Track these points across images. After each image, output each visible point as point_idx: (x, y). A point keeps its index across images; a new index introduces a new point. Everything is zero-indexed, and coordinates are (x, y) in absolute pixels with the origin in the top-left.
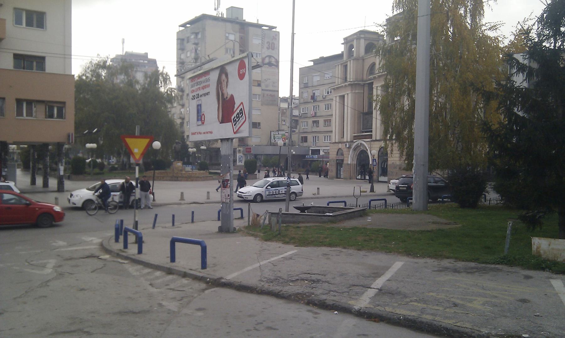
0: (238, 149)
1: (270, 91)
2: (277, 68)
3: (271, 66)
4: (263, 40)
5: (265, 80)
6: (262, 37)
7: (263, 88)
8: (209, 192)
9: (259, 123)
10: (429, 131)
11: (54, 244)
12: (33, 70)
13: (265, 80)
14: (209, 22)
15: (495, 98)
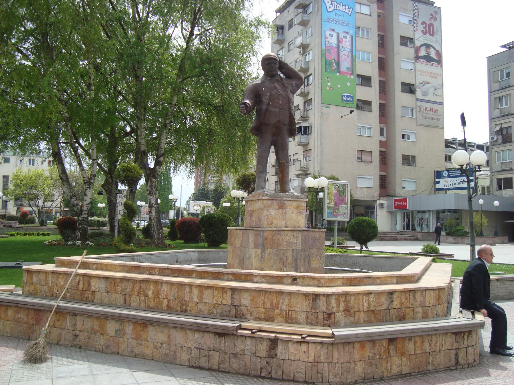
0: (378, 201)
1: (430, 102)
2: (439, 66)
3: (430, 62)
4: (415, 18)
5: (422, 83)
7: (418, 98)
8: (305, 133)
9: (414, 157)
10: (277, 291)
12: (33, 223)
13: (422, 83)
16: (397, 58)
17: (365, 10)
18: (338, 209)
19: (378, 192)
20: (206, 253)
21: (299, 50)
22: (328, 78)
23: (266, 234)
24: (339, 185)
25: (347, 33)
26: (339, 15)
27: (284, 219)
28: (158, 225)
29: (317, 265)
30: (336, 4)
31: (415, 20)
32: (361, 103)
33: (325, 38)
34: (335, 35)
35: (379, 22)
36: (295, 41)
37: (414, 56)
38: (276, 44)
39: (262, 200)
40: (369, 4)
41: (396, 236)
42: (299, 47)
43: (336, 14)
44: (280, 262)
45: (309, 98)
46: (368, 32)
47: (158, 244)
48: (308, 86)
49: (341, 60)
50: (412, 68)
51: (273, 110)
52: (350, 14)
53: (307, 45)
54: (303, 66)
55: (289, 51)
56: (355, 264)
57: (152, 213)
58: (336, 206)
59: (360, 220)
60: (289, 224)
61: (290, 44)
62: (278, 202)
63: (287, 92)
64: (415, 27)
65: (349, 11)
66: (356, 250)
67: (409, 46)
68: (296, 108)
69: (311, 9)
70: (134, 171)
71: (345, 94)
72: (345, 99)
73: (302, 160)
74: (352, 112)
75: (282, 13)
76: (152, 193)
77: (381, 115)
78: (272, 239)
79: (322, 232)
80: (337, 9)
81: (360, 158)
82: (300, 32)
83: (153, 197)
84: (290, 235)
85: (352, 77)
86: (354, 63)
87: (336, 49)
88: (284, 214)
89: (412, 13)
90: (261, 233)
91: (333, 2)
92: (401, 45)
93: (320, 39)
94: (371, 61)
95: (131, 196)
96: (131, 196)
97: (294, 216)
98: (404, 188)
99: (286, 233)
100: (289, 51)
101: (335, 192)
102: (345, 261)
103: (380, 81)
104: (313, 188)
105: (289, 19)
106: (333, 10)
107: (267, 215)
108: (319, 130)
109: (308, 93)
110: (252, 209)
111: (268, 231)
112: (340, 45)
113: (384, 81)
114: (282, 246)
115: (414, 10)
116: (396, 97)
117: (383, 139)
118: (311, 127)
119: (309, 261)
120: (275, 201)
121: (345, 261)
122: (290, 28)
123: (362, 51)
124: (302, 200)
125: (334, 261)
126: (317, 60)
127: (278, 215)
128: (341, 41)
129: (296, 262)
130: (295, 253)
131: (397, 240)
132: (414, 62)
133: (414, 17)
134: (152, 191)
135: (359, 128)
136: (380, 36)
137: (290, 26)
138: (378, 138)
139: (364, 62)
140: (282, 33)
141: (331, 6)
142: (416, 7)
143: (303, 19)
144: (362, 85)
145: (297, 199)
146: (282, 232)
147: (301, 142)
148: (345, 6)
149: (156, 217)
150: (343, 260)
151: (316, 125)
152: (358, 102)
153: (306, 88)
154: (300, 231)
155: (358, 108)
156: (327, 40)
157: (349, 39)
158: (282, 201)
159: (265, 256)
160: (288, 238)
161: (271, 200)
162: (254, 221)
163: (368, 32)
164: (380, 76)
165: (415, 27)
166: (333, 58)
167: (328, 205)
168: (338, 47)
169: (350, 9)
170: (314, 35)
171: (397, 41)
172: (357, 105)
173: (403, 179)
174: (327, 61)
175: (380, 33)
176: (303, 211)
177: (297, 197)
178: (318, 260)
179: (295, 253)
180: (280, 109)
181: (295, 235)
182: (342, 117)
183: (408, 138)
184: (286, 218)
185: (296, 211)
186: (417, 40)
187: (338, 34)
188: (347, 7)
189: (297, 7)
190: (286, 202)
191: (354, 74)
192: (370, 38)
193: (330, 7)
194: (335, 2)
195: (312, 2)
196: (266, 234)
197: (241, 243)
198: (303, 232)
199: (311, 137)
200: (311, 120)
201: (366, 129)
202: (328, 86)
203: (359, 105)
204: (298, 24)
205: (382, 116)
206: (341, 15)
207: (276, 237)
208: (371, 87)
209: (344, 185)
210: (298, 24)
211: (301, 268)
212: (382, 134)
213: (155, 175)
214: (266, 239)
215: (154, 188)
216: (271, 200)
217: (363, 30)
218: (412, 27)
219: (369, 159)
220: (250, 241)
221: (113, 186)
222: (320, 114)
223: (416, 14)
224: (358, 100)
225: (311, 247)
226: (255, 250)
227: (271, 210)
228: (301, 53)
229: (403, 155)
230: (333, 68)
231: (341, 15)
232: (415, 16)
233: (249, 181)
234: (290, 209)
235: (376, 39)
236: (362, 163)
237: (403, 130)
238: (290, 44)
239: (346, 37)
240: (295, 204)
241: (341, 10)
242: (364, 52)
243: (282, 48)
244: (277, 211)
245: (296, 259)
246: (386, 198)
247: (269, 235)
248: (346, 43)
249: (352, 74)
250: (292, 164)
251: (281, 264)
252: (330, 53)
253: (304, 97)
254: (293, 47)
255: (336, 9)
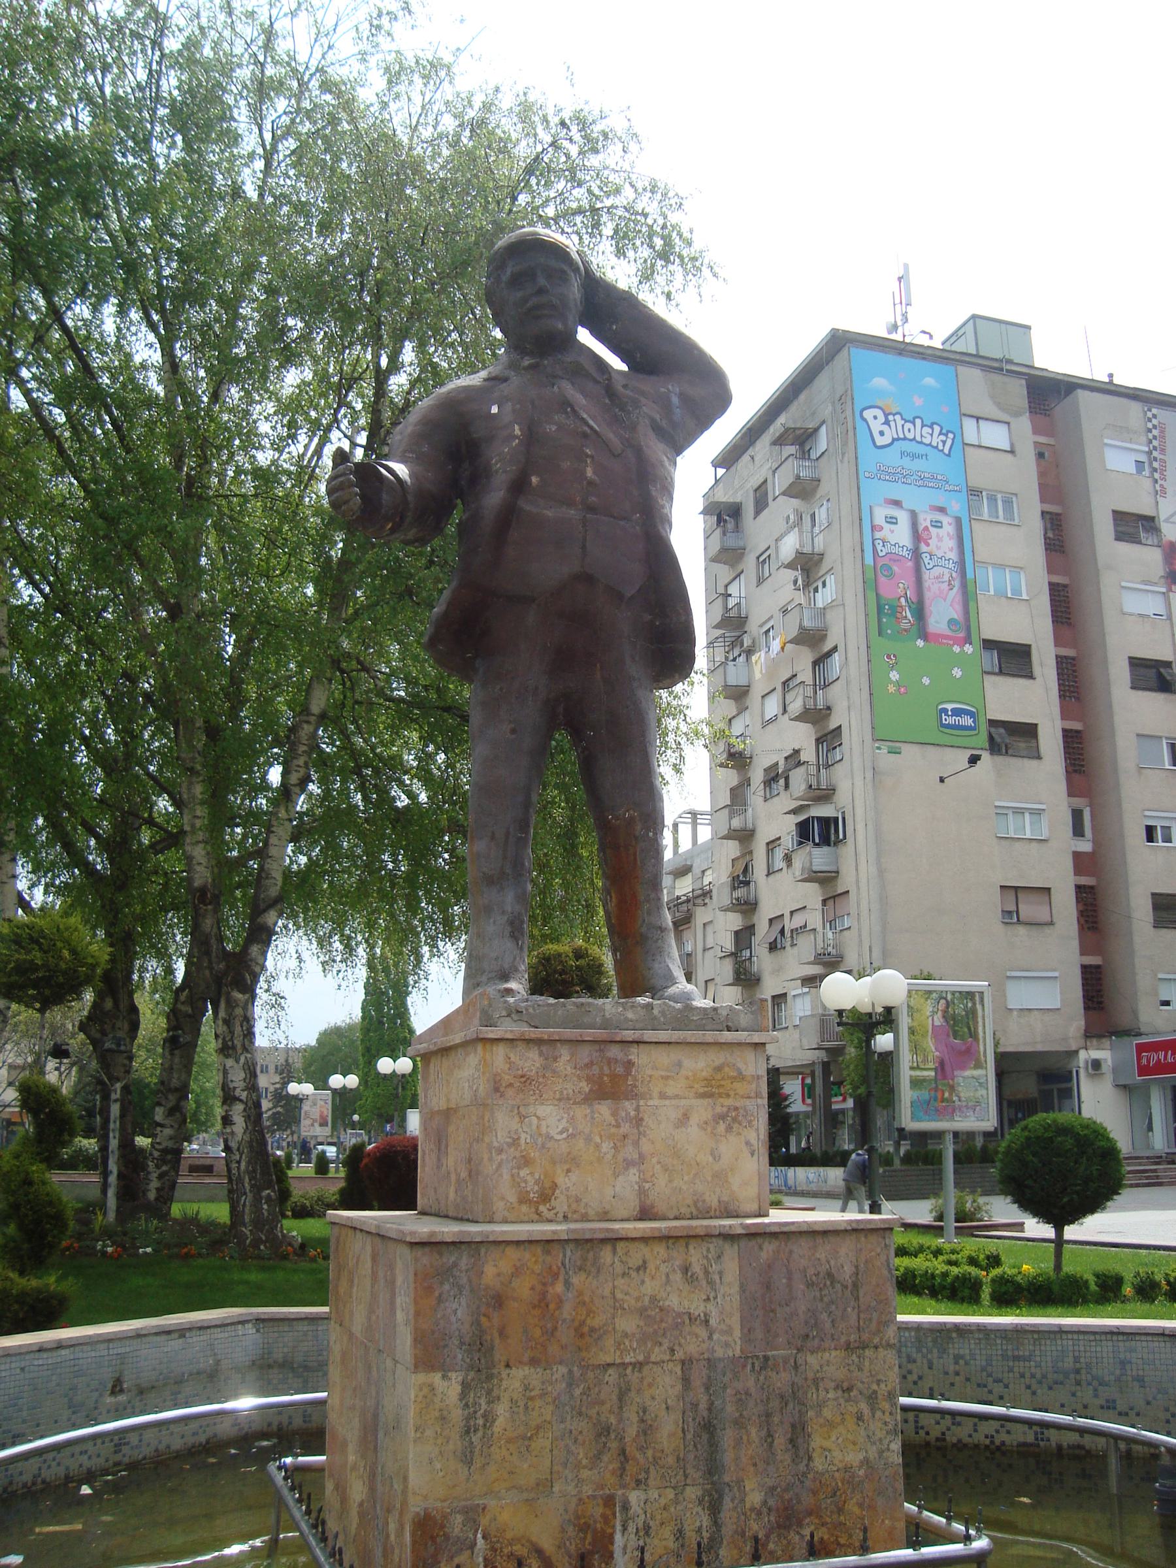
0: (1083, 1055)
4: (1155, 454)
6: (1150, 442)
8: (825, 841)
11: (266, 1538)
14: (859, 356)
15: (320, 1276)
16: (1108, 583)
17: (995, 435)
18: (952, 1088)
19: (1077, 1024)
20: (303, 1327)
21: (790, 575)
22: (889, 657)
23: (493, 1270)
24: (949, 997)
25: (942, 510)
26: (914, 456)
27: (629, 1164)
28: (254, 1171)
29: (853, 1458)
30: (900, 422)
31: (1155, 459)
32: (1002, 730)
33: (874, 528)
34: (903, 517)
35: (1042, 474)
36: (777, 548)
37: (1162, 573)
38: (719, 562)
39: (480, 1047)
40: (1005, 417)
41: (1155, 1171)
42: (790, 566)
43: (902, 453)
44: (598, 1457)
45: (833, 725)
46: (1008, 503)
47: (256, 1243)
48: (825, 686)
49: (928, 595)
50: (1161, 610)
51: (549, 513)
52: (946, 451)
53: (817, 557)
54: (807, 623)
55: (760, 581)
56: (1066, 1374)
57: (231, 1123)
58: (944, 1077)
59: (1047, 1127)
60: (661, 1191)
61: (761, 559)
62: (585, 1054)
63: (633, 428)
64: (1156, 481)
65: (944, 442)
66: (1029, 1240)
67: (1144, 541)
68: (792, 762)
69: (822, 442)
70: (59, 944)
71: (949, 706)
72: (951, 720)
73: (820, 929)
74: (974, 760)
75: (733, 468)
76: (234, 1048)
77: (1070, 769)
78: (542, 1302)
79: (873, 1238)
80: (905, 439)
81: (1010, 912)
82: (792, 517)
83: (237, 1061)
84: (664, 1268)
85: (968, 649)
86: (972, 604)
87: (910, 564)
88: (625, 1128)
89: (1144, 439)
90: (464, 1262)
91: (891, 418)
92: (1118, 539)
93: (857, 534)
94: (1025, 597)
95: (177, 1060)
96: (177, 1060)
97: (693, 1139)
98: (1166, 1003)
99: (638, 1253)
100: (760, 581)
101: (937, 1023)
102: (1016, 1358)
103: (1061, 661)
104: (854, 1010)
105: (756, 481)
106: (894, 440)
107: (515, 1142)
108: (870, 827)
109: (829, 708)
110: (443, 1105)
111: (510, 1251)
112: (923, 548)
113: (1073, 659)
114: (609, 1342)
115: (1150, 431)
116: (1116, 708)
117: (1085, 846)
118: (844, 819)
119: (798, 1433)
120: (565, 1053)
121: (1016, 1358)
122: (759, 510)
123: (994, 565)
124: (742, 1036)
125: (957, 1358)
126: (850, 600)
127: (588, 1140)
128: (925, 535)
129: (713, 1445)
130: (697, 1382)
131: (1160, 1184)
132: (1164, 590)
133: (1150, 453)
134: (232, 1040)
135: (1001, 812)
136: (1048, 517)
137: (761, 504)
138: (1065, 844)
139: (1003, 599)
140: (737, 528)
141: (885, 428)
142: (1155, 422)
143: (798, 477)
144: (1001, 672)
145: (710, 1036)
146: (606, 1255)
147: (815, 868)
148: (931, 427)
149: (247, 1138)
150: (1004, 1357)
151: (859, 812)
152: (993, 730)
153: (820, 693)
154: (728, 1237)
155: (994, 747)
156: (878, 535)
157: (948, 528)
158: (614, 1052)
159: (489, 1418)
160: (650, 1287)
161: (539, 1042)
162: (453, 1177)
163: (1008, 503)
164: (1058, 641)
165: (1156, 481)
166: (900, 591)
167: (914, 1073)
168: (916, 555)
169: (946, 435)
170: (836, 526)
171: (1104, 527)
172: (991, 738)
173: (1161, 976)
174: (883, 602)
175: (1049, 508)
176: (750, 1104)
177: (711, 1019)
178: (860, 1418)
179: (697, 1382)
180: (592, 509)
181: (697, 1268)
182: (942, 780)
183: (1168, 839)
184: (642, 1157)
185: (702, 1111)
186: (1167, 520)
187: (914, 515)
188: (937, 429)
189: (779, 442)
190: (641, 1058)
191: (975, 638)
192: (1016, 522)
193: (882, 433)
194: (898, 417)
195: (823, 422)
196: (493, 1270)
197: (369, 1319)
198: (753, 1243)
199: (847, 851)
200: (843, 797)
201: (1027, 815)
202: (892, 682)
203: (998, 739)
204: (784, 494)
205: (1075, 771)
206: (920, 456)
207: (567, 1284)
208: (1030, 676)
209: (970, 995)
210: (784, 494)
211: (749, 1485)
212: (1078, 830)
213: (244, 979)
214: (499, 1301)
215: (238, 1030)
216: (539, 1042)
217: (992, 499)
218: (1147, 484)
219: (1042, 914)
220: (400, 1316)
221: (119, 1024)
222: (869, 775)
223: (1155, 443)
224: (992, 723)
225: (804, 1342)
226: (421, 1378)
227: (545, 1110)
228: (800, 582)
229: (1153, 894)
230: (904, 625)
231: (920, 456)
232: (1155, 448)
233: (564, 982)
234: (663, 1096)
235: (1035, 526)
236: (1021, 930)
237: (1147, 813)
238: (761, 559)
239: (938, 525)
240: (699, 1064)
241: (918, 438)
242: (1002, 567)
243: (739, 575)
244: (581, 1112)
245: (709, 1428)
246: (1106, 1042)
247: (517, 1272)
248: (942, 543)
249: (968, 640)
250: (788, 944)
251: (609, 1462)
252: (891, 575)
253: (814, 723)
254: (774, 567)
255: (901, 436)
